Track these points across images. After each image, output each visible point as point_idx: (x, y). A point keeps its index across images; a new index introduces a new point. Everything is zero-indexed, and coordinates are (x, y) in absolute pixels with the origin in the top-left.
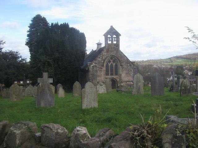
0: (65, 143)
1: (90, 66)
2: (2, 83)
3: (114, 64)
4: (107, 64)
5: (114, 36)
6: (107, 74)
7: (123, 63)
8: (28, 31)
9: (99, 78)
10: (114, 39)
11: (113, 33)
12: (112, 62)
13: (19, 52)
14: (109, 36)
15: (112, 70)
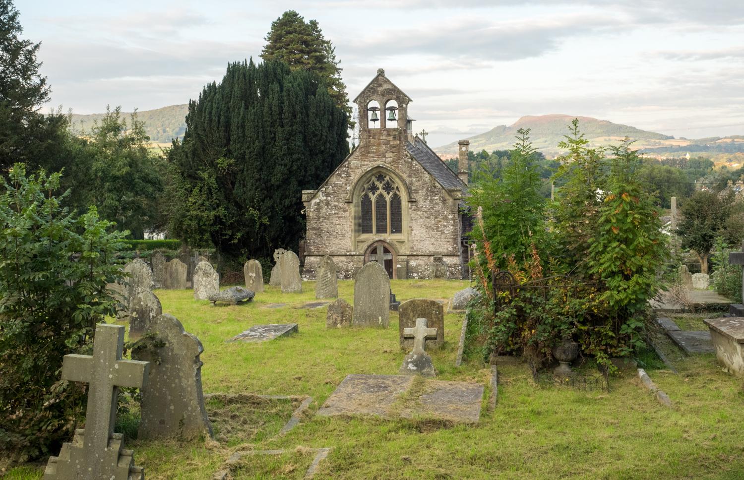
0: (733, 316)
1: (309, 201)
2: (2, 280)
3: (388, 198)
4: (366, 196)
5: (393, 103)
6: (363, 226)
7: (416, 192)
8: (269, 33)
9: (337, 241)
10: (370, 113)
11: (16, 13)
12: (380, 191)
13: (127, 109)
14: (373, 104)
15: (381, 217)
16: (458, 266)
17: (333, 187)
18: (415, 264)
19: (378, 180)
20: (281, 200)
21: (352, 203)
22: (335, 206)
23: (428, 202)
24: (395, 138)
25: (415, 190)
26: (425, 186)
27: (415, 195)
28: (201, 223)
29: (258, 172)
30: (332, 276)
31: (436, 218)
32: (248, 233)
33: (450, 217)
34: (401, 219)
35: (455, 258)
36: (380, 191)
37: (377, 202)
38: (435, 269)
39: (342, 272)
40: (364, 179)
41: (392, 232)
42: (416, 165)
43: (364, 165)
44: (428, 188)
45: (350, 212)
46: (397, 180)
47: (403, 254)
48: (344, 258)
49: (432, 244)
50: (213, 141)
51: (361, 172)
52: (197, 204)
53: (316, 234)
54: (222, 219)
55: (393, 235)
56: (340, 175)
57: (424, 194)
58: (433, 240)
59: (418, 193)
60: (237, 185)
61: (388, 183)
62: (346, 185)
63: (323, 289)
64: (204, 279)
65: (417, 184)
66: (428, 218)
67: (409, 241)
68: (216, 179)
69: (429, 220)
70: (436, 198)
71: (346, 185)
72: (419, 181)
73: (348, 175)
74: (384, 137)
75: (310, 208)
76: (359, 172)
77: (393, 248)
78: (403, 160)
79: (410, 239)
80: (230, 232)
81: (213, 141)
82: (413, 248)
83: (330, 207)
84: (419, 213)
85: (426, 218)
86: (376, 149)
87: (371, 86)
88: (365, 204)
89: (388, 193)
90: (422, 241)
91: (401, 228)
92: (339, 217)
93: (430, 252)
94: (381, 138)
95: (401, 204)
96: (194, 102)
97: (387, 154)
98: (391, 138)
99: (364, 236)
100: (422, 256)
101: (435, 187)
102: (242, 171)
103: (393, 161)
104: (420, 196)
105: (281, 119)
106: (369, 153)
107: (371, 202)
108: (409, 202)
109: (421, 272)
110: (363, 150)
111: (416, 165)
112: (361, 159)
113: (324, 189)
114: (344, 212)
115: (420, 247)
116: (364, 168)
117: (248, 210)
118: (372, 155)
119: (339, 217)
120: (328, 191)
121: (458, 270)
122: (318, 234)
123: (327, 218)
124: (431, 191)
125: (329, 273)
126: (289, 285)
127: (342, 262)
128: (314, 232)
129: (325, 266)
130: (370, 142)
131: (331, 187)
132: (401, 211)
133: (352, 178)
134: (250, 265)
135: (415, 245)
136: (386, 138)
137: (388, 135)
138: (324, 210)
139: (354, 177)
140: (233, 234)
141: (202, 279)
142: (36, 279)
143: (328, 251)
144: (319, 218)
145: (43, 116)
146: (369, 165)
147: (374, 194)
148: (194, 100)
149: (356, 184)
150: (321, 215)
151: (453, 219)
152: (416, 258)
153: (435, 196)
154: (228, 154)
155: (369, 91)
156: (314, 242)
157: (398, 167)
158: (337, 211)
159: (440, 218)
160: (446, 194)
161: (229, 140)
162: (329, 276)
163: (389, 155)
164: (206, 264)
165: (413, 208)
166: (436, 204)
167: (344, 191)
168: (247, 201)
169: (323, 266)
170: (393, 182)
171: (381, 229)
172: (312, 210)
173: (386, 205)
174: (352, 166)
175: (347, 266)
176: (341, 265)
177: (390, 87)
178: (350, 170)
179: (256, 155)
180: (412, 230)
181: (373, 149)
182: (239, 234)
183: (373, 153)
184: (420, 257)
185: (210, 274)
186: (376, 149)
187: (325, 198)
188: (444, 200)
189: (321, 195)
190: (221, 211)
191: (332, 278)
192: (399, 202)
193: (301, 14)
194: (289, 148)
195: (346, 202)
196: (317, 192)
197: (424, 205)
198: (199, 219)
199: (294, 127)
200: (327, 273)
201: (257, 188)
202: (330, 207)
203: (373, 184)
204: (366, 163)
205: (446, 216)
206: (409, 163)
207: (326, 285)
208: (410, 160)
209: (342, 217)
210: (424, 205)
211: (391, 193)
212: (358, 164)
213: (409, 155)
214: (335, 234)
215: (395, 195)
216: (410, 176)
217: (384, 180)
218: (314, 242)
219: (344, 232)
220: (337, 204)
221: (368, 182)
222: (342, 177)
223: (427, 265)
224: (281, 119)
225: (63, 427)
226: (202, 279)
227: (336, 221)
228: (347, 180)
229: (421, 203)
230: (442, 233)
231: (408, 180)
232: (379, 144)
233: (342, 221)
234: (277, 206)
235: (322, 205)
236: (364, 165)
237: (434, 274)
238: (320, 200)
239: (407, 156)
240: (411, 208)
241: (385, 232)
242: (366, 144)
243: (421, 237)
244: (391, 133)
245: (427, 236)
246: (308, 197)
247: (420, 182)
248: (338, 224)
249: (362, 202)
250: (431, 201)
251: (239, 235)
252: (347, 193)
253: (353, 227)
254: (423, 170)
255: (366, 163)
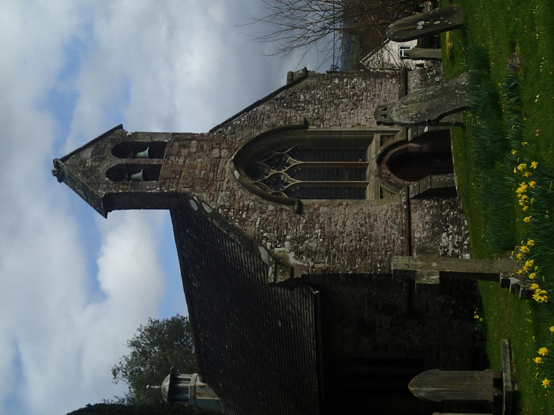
22: (305, 228)
56: (243, 221)
71: (264, 212)
98: (184, 152)
138: (313, 245)
142: (148, 368)
145: (127, 133)
172: (311, 264)
187: (287, 243)
193: (173, 316)
220: (301, 226)
225: (413, 123)
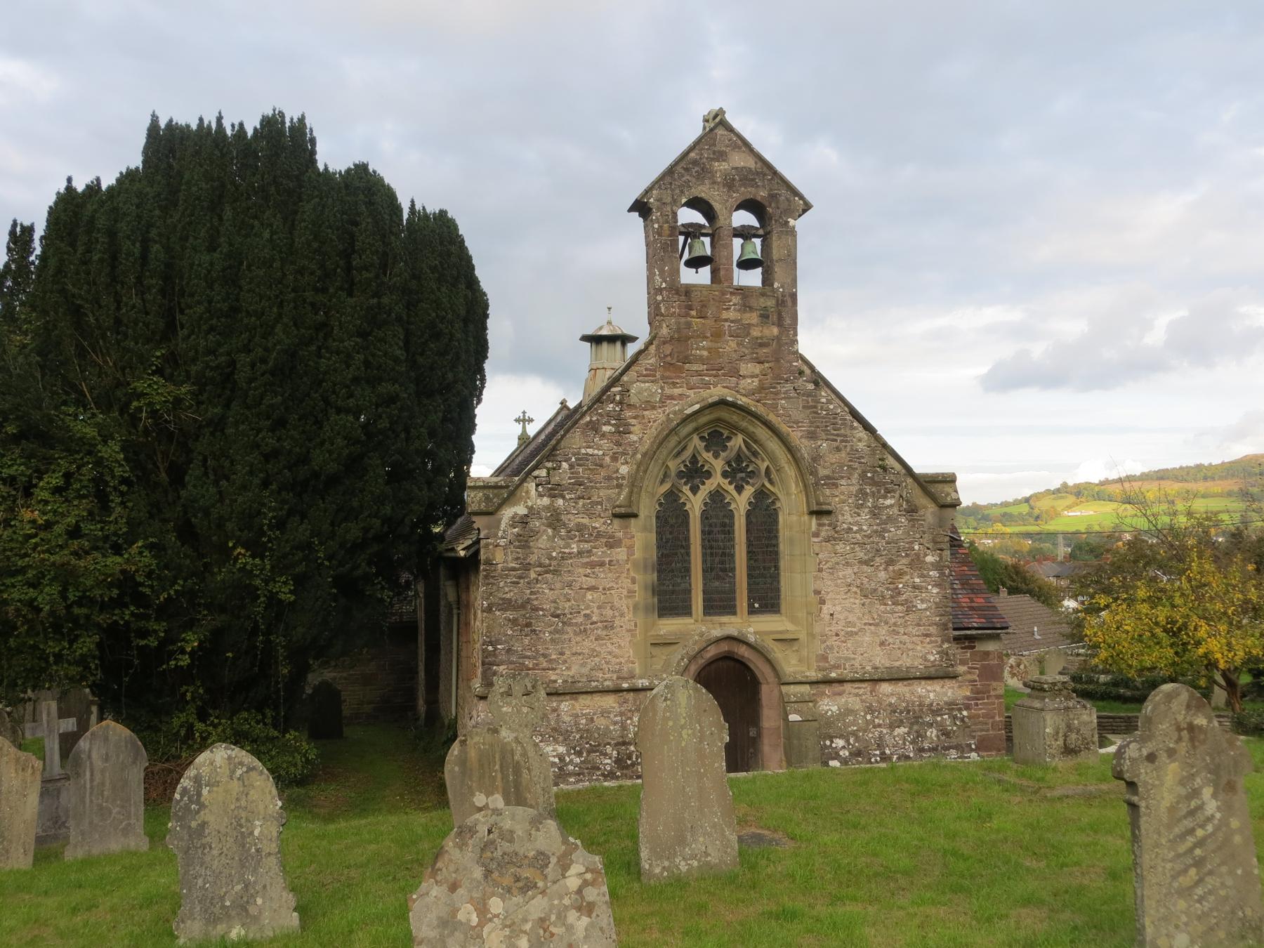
3: (741, 503)
7: (832, 482)
9: (588, 644)
15: (718, 563)
16: (960, 710)
17: (571, 467)
18: (835, 708)
19: (707, 449)
20: (332, 524)
21: (635, 516)
22: (580, 528)
23: (865, 516)
24: (765, 317)
25: (828, 477)
26: (856, 465)
27: (828, 492)
28: (72, 596)
29: (272, 429)
30: (1227, 809)
31: (890, 562)
32: (217, 634)
33: (929, 559)
34: (777, 568)
35: (948, 683)
36: (717, 481)
37: (705, 516)
38: (1063, 726)
39: (609, 749)
40: (674, 440)
41: (752, 611)
42: (829, 402)
43: (672, 397)
44: (864, 472)
45: (630, 548)
46: (774, 445)
47: (800, 678)
48: (610, 701)
49: (882, 644)
50: (118, 322)
51: (662, 417)
52: (58, 529)
53: (514, 622)
54: (142, 584)
55: (755, 618)
57: (854, 489)
58: (883, 631)
59: (836, 485)
60: (194, 472)
61: (739, 458)
62: (614, 458)
63: (1185, 892)
64: (496, 905)
65: (833, 458)
66: (866, 563)
67: (812, 635)
68: (123, 449)
69: (869, 570)
70: (889, 502)
71: (614, 458)
72: (838, 449)
73: (623, 429)
74: (732, 315)
75: (496, 536)
76: (657, 417)
77: (769, 661)
78: (789, 386)
79: (817, 629)
80: (160, 627)
81: (118, 322)
82: (824, 658)
83: (563, 532)
84: (840, 547)
85: (862, 562)
86: (709, 350)
87: (692, 155)
88: (666, 521)
89: (739, 489)
90: (851, 634)
91: (778, 597)
92: (592, 565)
93: (876, 668)
94: (725, 315)
95: (776, 522)
96: (29, 231)
97: (743, 365)
98: (753, 318)
99: (670, 626)
100: (852, 681)
101: (884, 469)
102: (218, 425)
103: (761, 388)
104: (841, 497)
105: (349, 268)
106: (686, 360)
107: (686, 515)
108: (812, 513)
109: (854, 734)
110: (668, 349)
111: (829, 402)
112: (663, 378)
113: (543, 473)
114: (610, 546)
115: (846, 654)
116: (673, 406)
117: (226, 554)
118: (695, 367)
119: (592, 565)
120: (556, 479)
121: (962, 720)
122: (522, 621)
123: (551, 569)
124: (873, 482)
125: (1207, 792)
126: (681, 841)
127: (605, 713)
128: (510, 615)
129: (1183, 747)
130: (689, 325)
131: (565, 465)
132: (777, 545)
133: (634, 438)
134: (473, 754)
135: (831, 648)
136: (737, 316)
137: (746, 307)
138: (543, 542)
139: (641, 435)
140: (170, 639)
141: (482, 910)
143: (558, 678)
144: (527, 567)
146: (691, 399)
147: (695, 490)
148: (27, 223)
149: (650, 456)
150: (533, 559)
151: (937, 566)
152: (837, 688)
153: (885, 497)
154: (171, 367)
155: (687, 170)
156: (509, 651)
157: (774, 407)
158: (587, 546)
159: (902, 563)
160: (917, 491)
161: (171, 327)
162: (1211, 806)
163: (748, 368)
164: (233, 764)
165: (823, 534)
166: (890, 519)
167: (609, 478)
168: (229, 526)
169: (1171, 753)
170: (755, 454)
171: (719, 604)
172: (502, 542)
173: (732, 525)
174: (634, 400)
175: (624, 727)
176: (601, 722)
177: (750, 163)
178: (628, 414)
179: (273, 374)
180: (823, 602)
181: (701, 349)
182: (189, 636)
183: (701, 360)
184: (848, 687)
185: (541, 860)
186: (709, 350)
187: (546, 501)
188: (912, 510)
189: (533, 492)
190: (138, 558)
191: (1224, 822)
192: (772, 516)
194: (367, 364)
195: (615, 516)
196: (523, 481)
197: (857, 523)
198: (66, 577)
199: (385, 300)
200: (1196, 793)
201: (265, 484)
202: (563, 532)
203: (694, 459)
204: (677, 391)
205: (918, 555)
206: (809, 394)
207: (1199, 863)
208: (811, 386)
209: (602, 564)
210: (857, 523)
211: (749, 491)
212: (652, 395)
213: (808, 371)
214: (580, 620)
215: (761, 495)
216: (812, 436)
217: (725, 448)
218: (509, 651)
219: (608, 612)
220: (586, 521)
221: (679, 454)
222: (603, 435)
223: (870, 709)
224: (349, 268)
226: (482, 910)
227: (582, 577)
228: (618, 444)
229: (846, 517)
230: (908, 611)
231: (805, 447)
232: (717, 335)
233: (604, 578)
234: (321, 543)
235: (536, 524)
236: (672, 397)
237: (1060, 742)
238: (531, 509)
239: (801, 373)
240: (816, 535)
241: (686, 611)
242: (678, 330)
243: (849, 624)
244: (753, 302)
245: (867, 619)
246: (487, 498)
247: (843, 454)
248: (590, 589)
249: (657, 517)
250: (875, 512)
251: (192, 641)
252: (619, 486)
253: (639, 597)
254: (849, 417)
255: (677, 391)
